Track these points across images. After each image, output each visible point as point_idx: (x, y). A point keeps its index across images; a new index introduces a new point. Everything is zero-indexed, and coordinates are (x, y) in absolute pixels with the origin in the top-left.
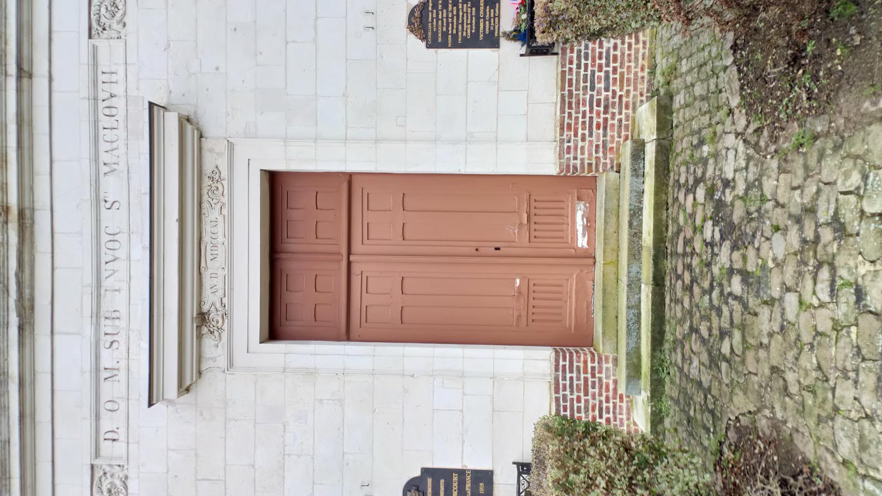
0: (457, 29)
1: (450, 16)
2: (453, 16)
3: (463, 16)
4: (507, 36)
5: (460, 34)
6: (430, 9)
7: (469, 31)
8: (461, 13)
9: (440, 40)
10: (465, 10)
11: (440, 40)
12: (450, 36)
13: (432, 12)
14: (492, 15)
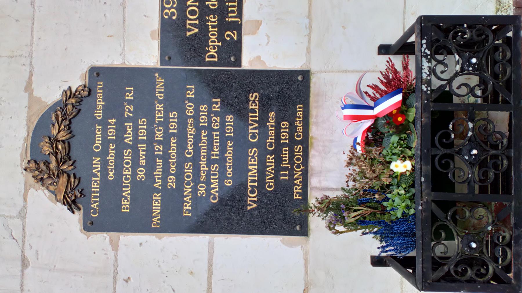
0: (180, 175)
1: (159, 136)
2: (167, 136)
3: (197, 139)
4: (338, 211)
5: (188, 189)
6: (99, 114)
7: (215, 182)
8: (191, 130)
9: (126, 205)
10: (203, 120)
11: (126, 205)
12: (157, 196)
13: (104, 124)
14: (285, 136)
